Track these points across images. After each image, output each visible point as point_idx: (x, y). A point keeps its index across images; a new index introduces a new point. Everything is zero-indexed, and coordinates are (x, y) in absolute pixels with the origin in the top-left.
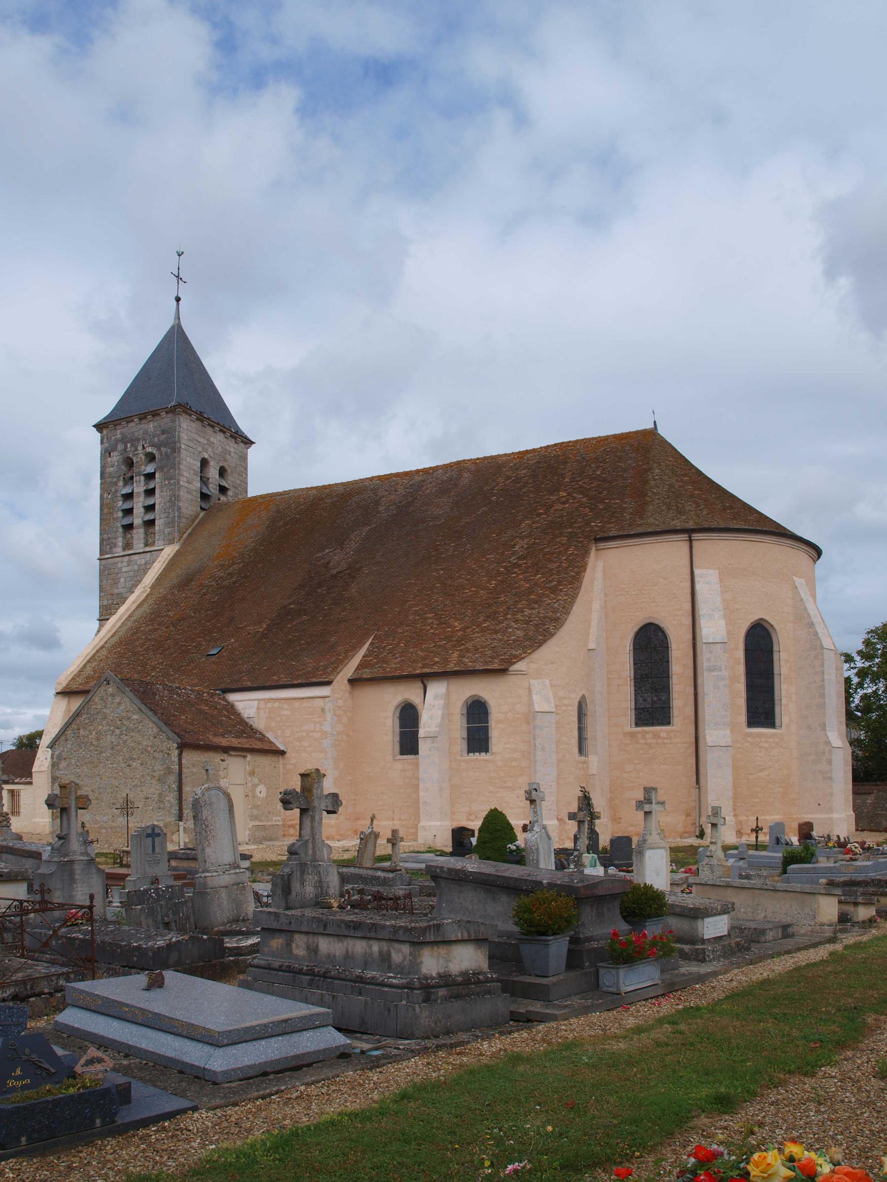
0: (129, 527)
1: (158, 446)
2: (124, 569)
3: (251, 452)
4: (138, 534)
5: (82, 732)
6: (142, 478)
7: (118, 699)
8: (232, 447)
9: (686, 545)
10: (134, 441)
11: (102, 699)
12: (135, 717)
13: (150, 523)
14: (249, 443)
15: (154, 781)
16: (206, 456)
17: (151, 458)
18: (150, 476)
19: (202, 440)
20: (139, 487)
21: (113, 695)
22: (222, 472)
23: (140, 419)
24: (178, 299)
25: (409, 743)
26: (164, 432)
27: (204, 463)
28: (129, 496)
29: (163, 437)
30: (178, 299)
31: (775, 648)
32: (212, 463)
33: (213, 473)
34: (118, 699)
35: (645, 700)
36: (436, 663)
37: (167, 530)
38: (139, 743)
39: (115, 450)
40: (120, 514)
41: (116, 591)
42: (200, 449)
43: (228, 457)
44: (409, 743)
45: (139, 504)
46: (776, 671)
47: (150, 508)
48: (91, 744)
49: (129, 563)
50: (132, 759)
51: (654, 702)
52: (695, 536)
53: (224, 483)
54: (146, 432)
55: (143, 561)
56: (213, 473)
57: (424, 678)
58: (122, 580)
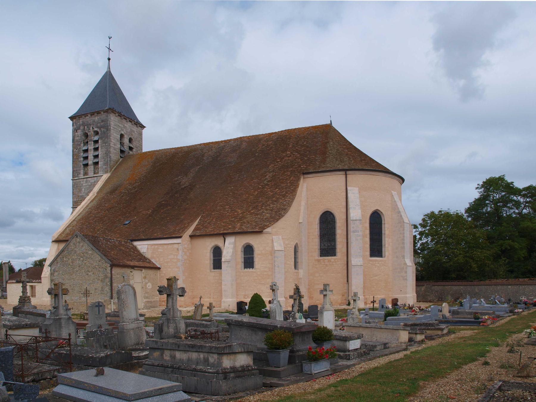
0: (86, 165)
1: (100, 128)
2: (84, 185)
3: (144, 131)
4: (91, 168)
5: (65, 259)
6: (92, 142)
7: (81, 244)
8: (135, 128)
9: (344, 177)
10: (88, 125)
11: (74, 244)
12: (90, 252)
13: (96, 164)
14: (143, 127)
15: (99, 282)
16: (123, 133)
17: (97, 133)
18: (96, 142)
19: (120, 125)
20: (91, 147)
21: (79, 242)
22: (130, 140)
23: (91, 115)
24: (109, 59)
25: (217, 264)
26: (102, 121)
27: (122, 136)
28: (86, 151)
29: (102, 124)
30: (109, 59)
31: (383, 222)
32: (125, 136)
33: (126, 141)
34: (81, 244)
35: (324, 245)
36: (230, 228)
37: (104, 167)
38: (92, 264)
39: (79, 129)
40: (82, 159)
41: (80, 195)
42: (120, 129)
43: (133, 133)
44: (217, 264)
45: (91, 155)
46: (383, 232)
47: (96, 157)
48: (69, 264)
49: (86, 182)
50: (88, 271)
51: (328, 246)
52: (348, 172)
53: (131, 146)
54: (94, 121)
55: (93, 181)
56: (126, 141)
57: (224, 235)
58: (83, 189)
